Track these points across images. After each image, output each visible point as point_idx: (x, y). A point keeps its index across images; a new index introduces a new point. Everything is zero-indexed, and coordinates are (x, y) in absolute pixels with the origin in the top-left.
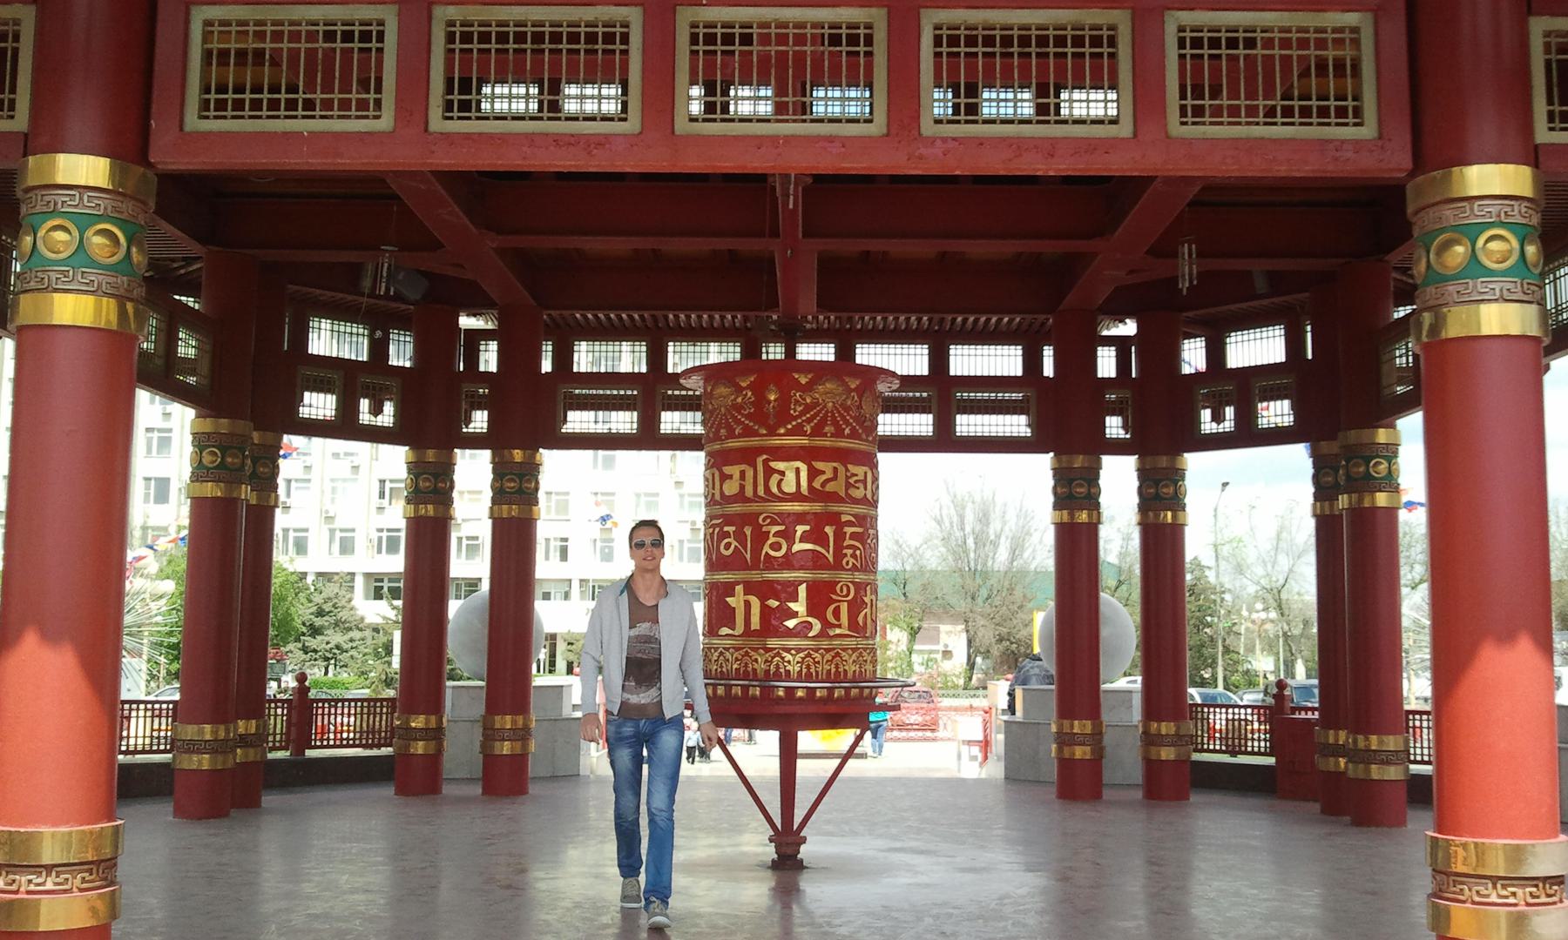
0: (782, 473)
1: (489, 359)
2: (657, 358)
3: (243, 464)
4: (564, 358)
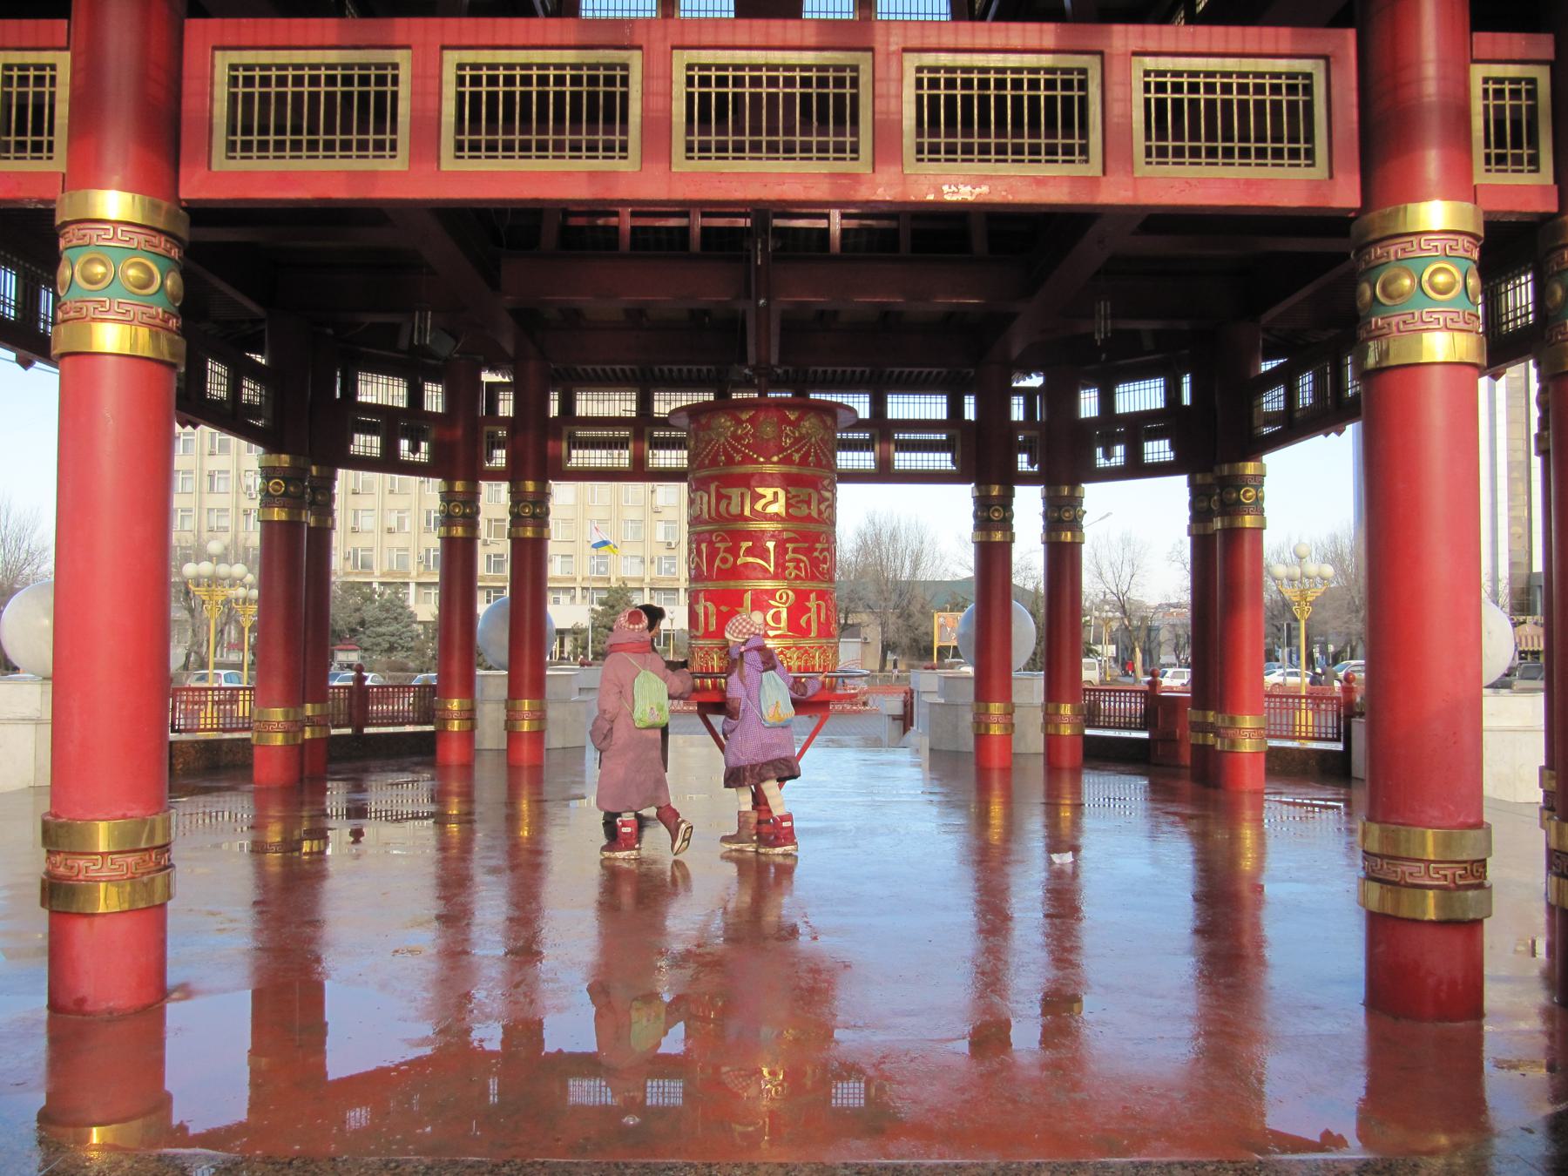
0: (729, 498)
1: (506, 407)
2: (645, 404)
3: (303, 493)
4: (567, 405)
